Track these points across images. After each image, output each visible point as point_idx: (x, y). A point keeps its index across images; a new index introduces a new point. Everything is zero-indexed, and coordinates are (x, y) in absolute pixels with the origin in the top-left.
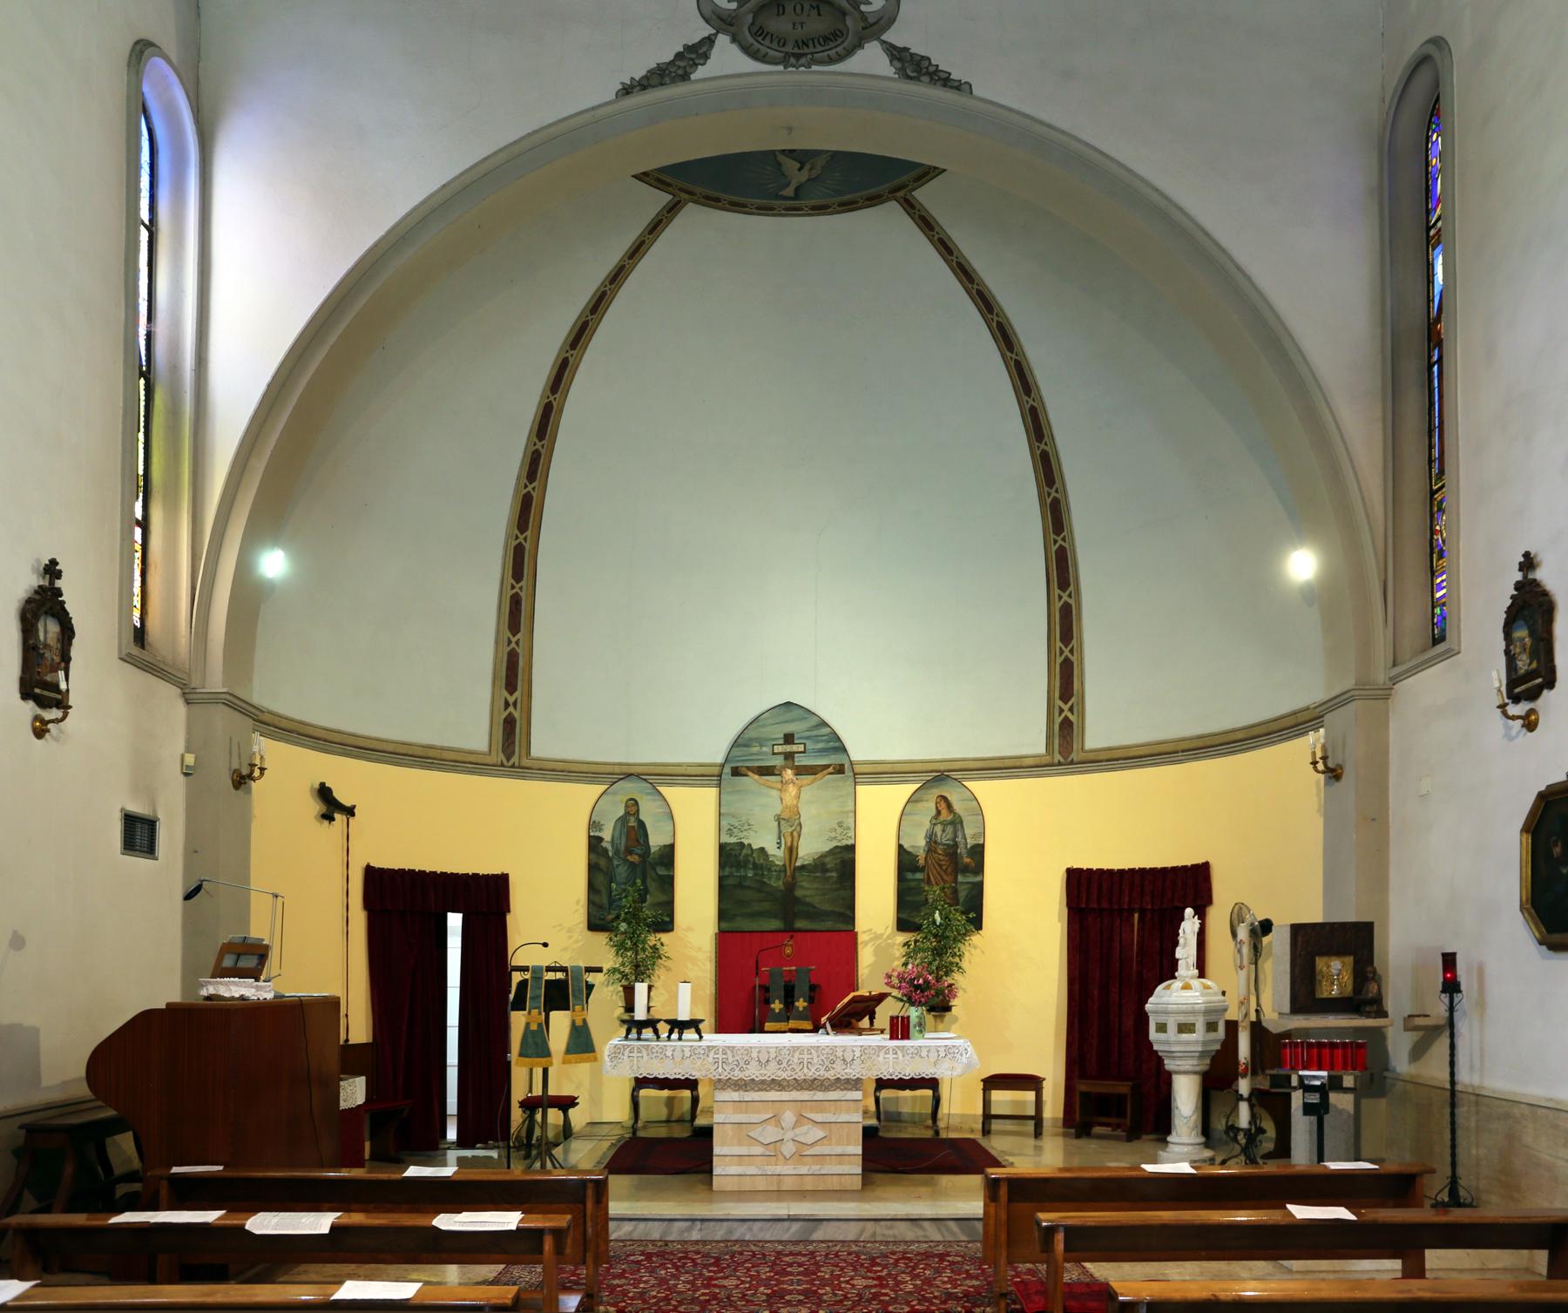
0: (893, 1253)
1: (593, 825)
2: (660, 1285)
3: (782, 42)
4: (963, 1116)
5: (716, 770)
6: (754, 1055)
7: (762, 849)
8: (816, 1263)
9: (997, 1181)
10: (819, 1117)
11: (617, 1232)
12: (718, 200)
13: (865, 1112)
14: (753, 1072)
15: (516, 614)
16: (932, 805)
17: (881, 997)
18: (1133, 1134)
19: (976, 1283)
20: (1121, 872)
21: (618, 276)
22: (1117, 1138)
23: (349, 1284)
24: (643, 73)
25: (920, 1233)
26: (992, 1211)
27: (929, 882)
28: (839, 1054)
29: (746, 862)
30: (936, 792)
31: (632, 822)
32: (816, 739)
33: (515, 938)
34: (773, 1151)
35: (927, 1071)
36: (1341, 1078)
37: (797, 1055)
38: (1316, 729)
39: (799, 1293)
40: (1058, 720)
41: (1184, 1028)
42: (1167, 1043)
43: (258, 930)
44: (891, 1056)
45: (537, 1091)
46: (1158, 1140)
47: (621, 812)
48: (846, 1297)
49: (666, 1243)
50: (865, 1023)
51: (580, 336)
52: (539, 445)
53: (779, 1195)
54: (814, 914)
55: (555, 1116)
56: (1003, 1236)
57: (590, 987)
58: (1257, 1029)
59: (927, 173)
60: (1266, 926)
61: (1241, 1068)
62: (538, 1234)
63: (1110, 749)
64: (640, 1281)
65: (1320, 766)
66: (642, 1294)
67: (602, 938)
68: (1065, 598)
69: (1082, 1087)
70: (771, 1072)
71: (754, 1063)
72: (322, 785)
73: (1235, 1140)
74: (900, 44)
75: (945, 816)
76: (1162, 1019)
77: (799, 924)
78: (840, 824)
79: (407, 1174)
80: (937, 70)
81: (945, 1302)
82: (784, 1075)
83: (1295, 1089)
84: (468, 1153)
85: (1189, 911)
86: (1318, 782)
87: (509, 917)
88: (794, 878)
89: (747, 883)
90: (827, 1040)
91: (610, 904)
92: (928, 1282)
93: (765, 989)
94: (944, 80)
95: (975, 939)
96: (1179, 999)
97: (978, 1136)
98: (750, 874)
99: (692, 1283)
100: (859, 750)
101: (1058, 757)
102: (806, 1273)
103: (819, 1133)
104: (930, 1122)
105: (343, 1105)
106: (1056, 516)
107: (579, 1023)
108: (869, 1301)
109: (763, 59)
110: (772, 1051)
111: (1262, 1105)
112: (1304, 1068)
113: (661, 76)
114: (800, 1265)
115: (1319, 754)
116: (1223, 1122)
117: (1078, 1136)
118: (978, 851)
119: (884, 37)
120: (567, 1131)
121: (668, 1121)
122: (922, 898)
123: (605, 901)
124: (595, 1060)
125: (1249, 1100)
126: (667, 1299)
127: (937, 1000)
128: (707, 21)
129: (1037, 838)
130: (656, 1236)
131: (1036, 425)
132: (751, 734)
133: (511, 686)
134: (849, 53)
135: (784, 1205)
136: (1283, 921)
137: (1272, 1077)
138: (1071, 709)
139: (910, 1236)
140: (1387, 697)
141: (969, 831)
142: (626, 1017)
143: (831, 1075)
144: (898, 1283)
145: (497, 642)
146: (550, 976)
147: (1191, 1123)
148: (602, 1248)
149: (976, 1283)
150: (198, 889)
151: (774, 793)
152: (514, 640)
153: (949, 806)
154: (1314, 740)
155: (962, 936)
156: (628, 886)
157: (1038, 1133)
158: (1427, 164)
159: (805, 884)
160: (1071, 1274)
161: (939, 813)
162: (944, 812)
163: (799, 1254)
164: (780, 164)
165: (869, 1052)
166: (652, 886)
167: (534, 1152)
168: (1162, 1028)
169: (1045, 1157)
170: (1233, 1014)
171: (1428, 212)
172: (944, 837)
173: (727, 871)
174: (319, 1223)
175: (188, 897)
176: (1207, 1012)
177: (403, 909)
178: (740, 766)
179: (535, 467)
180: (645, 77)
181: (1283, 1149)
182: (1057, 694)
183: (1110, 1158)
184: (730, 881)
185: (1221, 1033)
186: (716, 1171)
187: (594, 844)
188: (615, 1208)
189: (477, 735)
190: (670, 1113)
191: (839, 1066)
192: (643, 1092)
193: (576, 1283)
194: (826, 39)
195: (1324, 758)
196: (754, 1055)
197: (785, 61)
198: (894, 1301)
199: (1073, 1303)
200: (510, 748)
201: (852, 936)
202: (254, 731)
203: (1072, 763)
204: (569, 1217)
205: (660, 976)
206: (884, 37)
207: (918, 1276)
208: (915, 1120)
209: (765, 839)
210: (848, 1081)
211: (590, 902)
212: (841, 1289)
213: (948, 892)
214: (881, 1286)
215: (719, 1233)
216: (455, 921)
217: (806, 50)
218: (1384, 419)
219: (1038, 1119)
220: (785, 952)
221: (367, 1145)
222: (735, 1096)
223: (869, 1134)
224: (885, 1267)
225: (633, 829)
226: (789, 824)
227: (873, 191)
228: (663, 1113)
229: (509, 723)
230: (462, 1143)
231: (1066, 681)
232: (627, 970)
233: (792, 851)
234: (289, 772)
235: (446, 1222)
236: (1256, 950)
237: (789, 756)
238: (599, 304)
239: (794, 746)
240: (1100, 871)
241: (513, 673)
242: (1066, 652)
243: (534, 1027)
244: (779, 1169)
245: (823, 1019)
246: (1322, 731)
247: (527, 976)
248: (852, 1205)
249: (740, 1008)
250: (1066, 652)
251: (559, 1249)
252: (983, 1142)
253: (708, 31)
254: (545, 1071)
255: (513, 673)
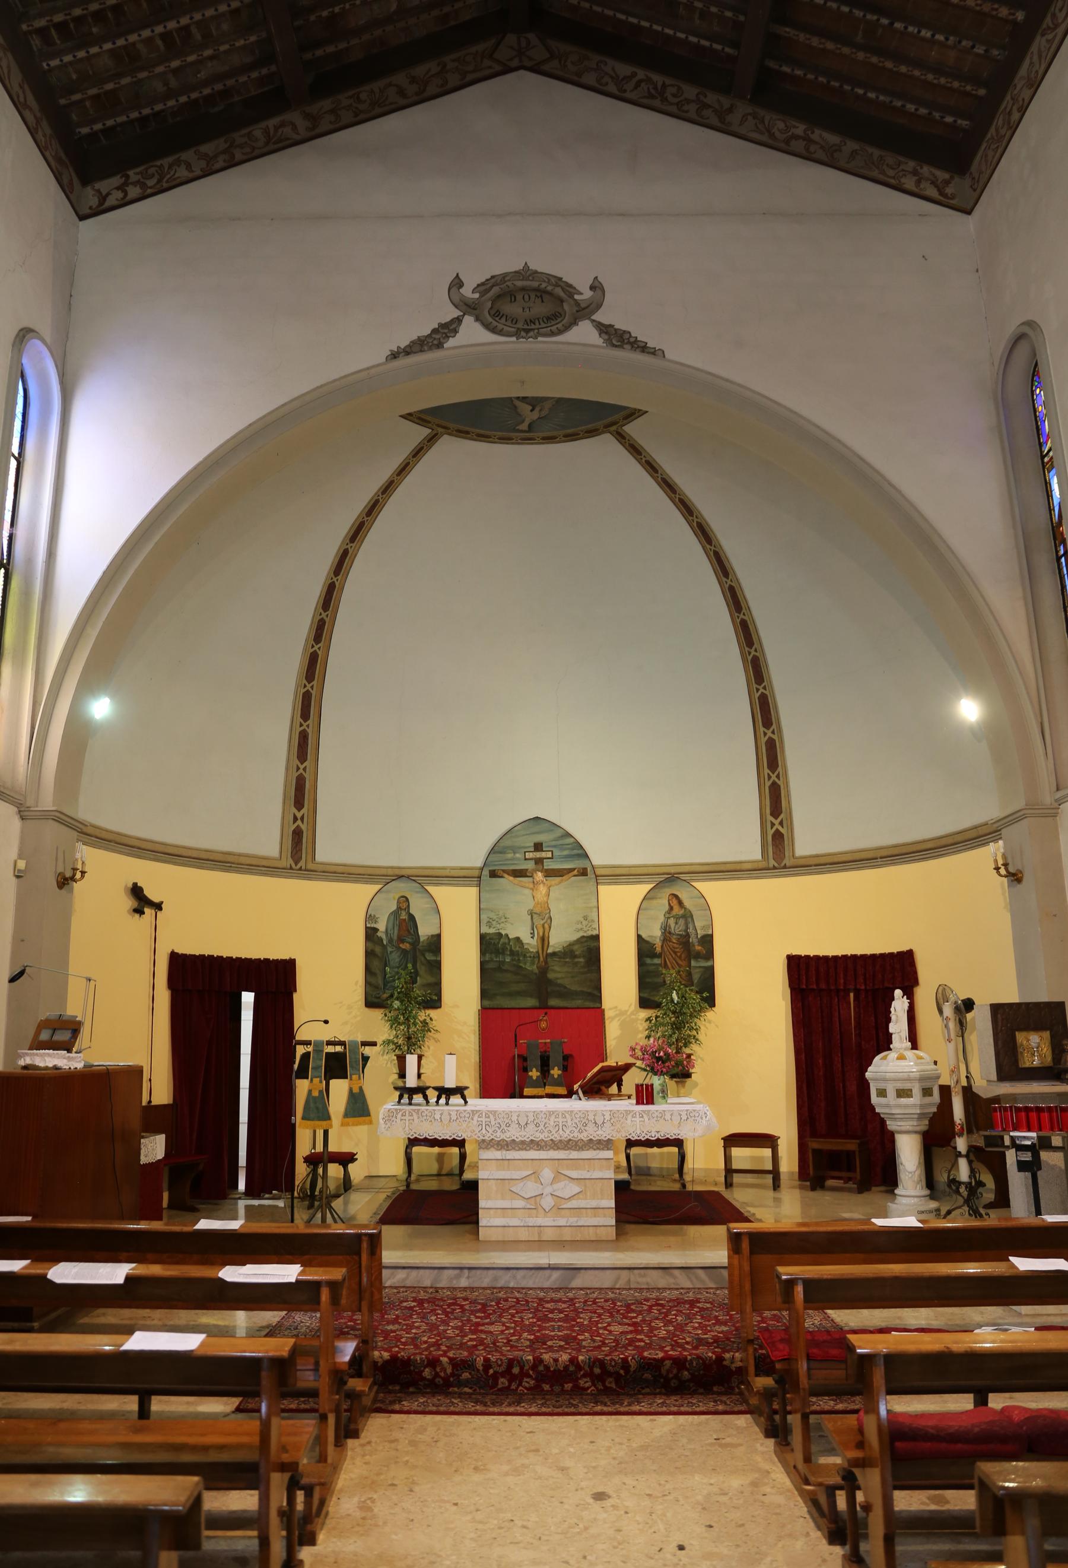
0: (647, 1300)
1: (369, 917)
2: (430, 1330)
3: (514, 321)
4: (706, 1170)
5: (476, 873)
6: (514, 1118)
7: (518, 939)
8: (576, 1310)
9: (738, 1236)
10: (574, 1174)
11: (390, 1279)
12: (467, 433)
13: (617, 1168)
14: (514, 1133)
15: (304, 746)
16: (665, 902)
17: (627, 1067)
18: (863, 1187)
19: (725, 1329)
20: (835, 958)
21: (388, 488)
22: (850, 1190)
23: (138, 1335)
24: (408, 343)
25: (671, 1280)
26: (736, 1262)
27: (666, 966)
28: (591, 1117)
29: (504, 949)
30: (668, 891)
31: (404, 916)
32: (561, 847)
33: (300, 1015)
34: (534, 1204)
35: (671, 1133)
36: (1050, 1138)
37: (552, 1118)
38: (996, 841)
39: (560, 1338)
40: (771, 832)
41: (902, 1093)
42: (888, 1106)
43: (73, 1009)
44: (638, 1119)
45: (319, 1148)
46: (887, 1192)
47: (394, 907)
48: (604, 1344)
49: (437, 1290)
50: (614, 1089)
51: (358, 532)
52: (324, 615)
53: (540, 1244)
54: (564, 993)
55: (335, 1170)
56: (748, 1287)
57: (366, 1059)
58: (968, 1093)
59: (633, 414)
60: (969, 1005)
61: (957, 1128)
62: (316, 1285)
63: (817, 856)
64: (412, 1327)
65: (1003, 871)
66: (414, 1339)
67: (377, 1014)
68: (769, 734)
69: (814, 1144)
70: (530, 1133)
71: (514, 1126)
72: (135, 885)
73: (958, 1192)
74: (607, 323)
75: (677, 910)
76: (881, 1085)
77: (553, 1002)
78: (585, 918)
79: (197, 1227)
80: (636, 340)
81: (696, 1348)
82: (542, 1137)
83: (1008, 1147)
84: (256, 1202)
85: (898, 993)
86: (1002, 884)
87: (295, 996)
88: (546, 962)
89: (505, 967)
90: (579, 1105)
91: (385, 985)
92: (680, 1328)
93: (523, 1059)
94: (643, 348)
95: (710, 1014)
96: (895, 1070)
97: (721, 1189)
98: (508, 959)
99: (461, 1329)
100: (599, 857)
101: (772, 863)
102: (566, 1319)
103: (576, 1189)
104: (677, 1176)
105: (144, 1160)
106: (757, 670)
107: (356, 1090)
108: (625, 1347)
109: (500, 333)
110: (531, 1116)
111: (979, 1160)
112: (1014, 1129)
113: (420, 345)
114: (561, 1311)
115: (1000, 862)
116: (945, 1176)
117: (813, 1189)
118: (708, 941)
119: (593, 317)
120: (347, 1184)
121: (439, 1175)
122: (660, 980)
123: (380, 982)
124: (371, 1123)
125: (967, 1156)
126: (437, 1345)
127: (676, 1070)
128: (456, 307)
129: (760, 934)
130: (427, 1283)
131: (735, 600)
132: (507, 842)
133: (299, 803)
134: (567, 328)
135: (546, 1254)
136: (983, 1001)
137: (986, 1137)
138: (781, 823)
139: (662, 1284)
140: (1055, 815)
141: (698, 924)
142: (400, 1084)
143: (584, 1136)
144: (652, 1329)
145: (287, 769)
146: (330, 1049)
147: (916, 1178)
148: (376, 1296)
149: (725, 1329)
150: (22, 973)
151: (527, 892)
152: (302, 767)
153: (680, 903)
154: (994, 850)
155: (697, 1013)
156: (402, 970)
157: (776, 1185)
158: (1035, 411)
159: (557, 968)
160: (813, 1320)
161: (671, 908)
162: (676, 908)
163: (560, 1300)
164: (516, 407)
165: (617, 1116)
166: (422, 970)
167: (317, 1203)
168: (882, 1093)
169: (783, 1210)
170: (945, 1080)
171: (1040, 445)
172: (677, 928)
173: (487, 957)
174: (115, 1273)
175: (12, 980)
176: (921, 1079)
177: (202, 989)
178: (496, 870)
179: (321, 631)
180: (409, 346)
181: (1002, 1200)
182: (768, 811)
183: (844, 1210)
184: (491, 966)
185: (936, 1097)
186: (482, 1222)
187: (371, 934)
188: (388, 1257)
189: (267, 840)
190: (441, 1168)
191: (591, 1128)
192: (415, 1149)
193: (353, 1328)
194: (548, 319)
195: (1006, 865)
196: (514, 1118)
197: (517, 334)
198: (649, 1346)
199: (815, 1351)
200: (298, 853)
201: (602, 1012)
202: (78, 840)
203: (785, 867)
204: (344, 1270)
205: (430, 1048)
206: (593, 317)
207: (670, 1322)
208: (663, 1175)
209: (519, 930)
210: (599, 1142)
211: (367, 983)
212: (599, 1335)
213: (684, 974)
214: (637, 1332)
215: (486, 1280)
216: (248, 998)
217: (533, 326)
218: (1025, 598)
219: (775, 1173)
220: (541, 1026)
221: (166, 1196)
222: (498, 1154)
223: (621, 1187)
224: (640, 1313)
225: (405, 923)
226: (541, 917)
227: (590, 426)
228: (434, 1168)
229: (297, 834)
230: (250, 1193)
231: (775, 801)
232: (400, 1042)
233: (544, 940)
234: (106, 875)
235: (232, 1274)
236: (962, 1024)
237: (539, 861)
238: (373, 509)
239: (541, 853)
240: (817, 958)
241: (301, 793)
242: (774, 777)
243: (316, 1094)
244: (540, 1221)
245: (576, 1087)
246: (1001, 842)
247: (310, 1049)
248: (607, 1254)
249: (503, 1076)
250: (774, 777)
251: (335, 1300)
252: (726, 1194)
253: (457, 313)
254: (326, 1133)
255: (301, 793)
